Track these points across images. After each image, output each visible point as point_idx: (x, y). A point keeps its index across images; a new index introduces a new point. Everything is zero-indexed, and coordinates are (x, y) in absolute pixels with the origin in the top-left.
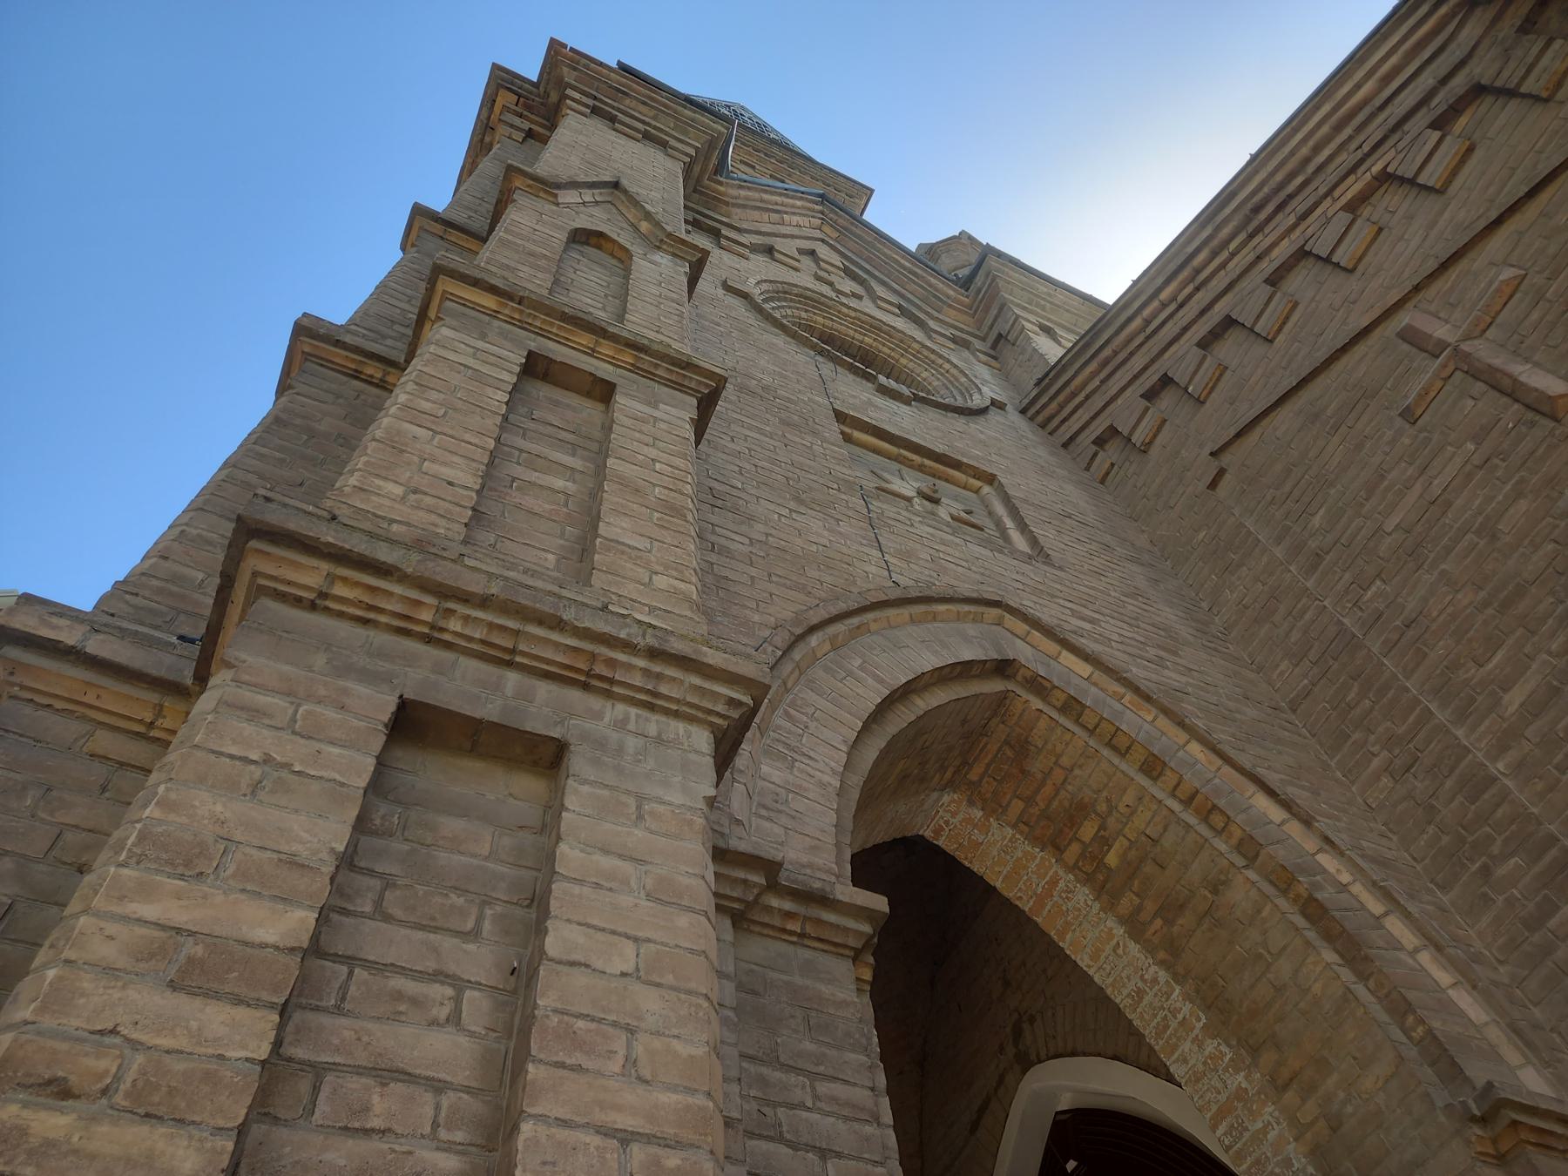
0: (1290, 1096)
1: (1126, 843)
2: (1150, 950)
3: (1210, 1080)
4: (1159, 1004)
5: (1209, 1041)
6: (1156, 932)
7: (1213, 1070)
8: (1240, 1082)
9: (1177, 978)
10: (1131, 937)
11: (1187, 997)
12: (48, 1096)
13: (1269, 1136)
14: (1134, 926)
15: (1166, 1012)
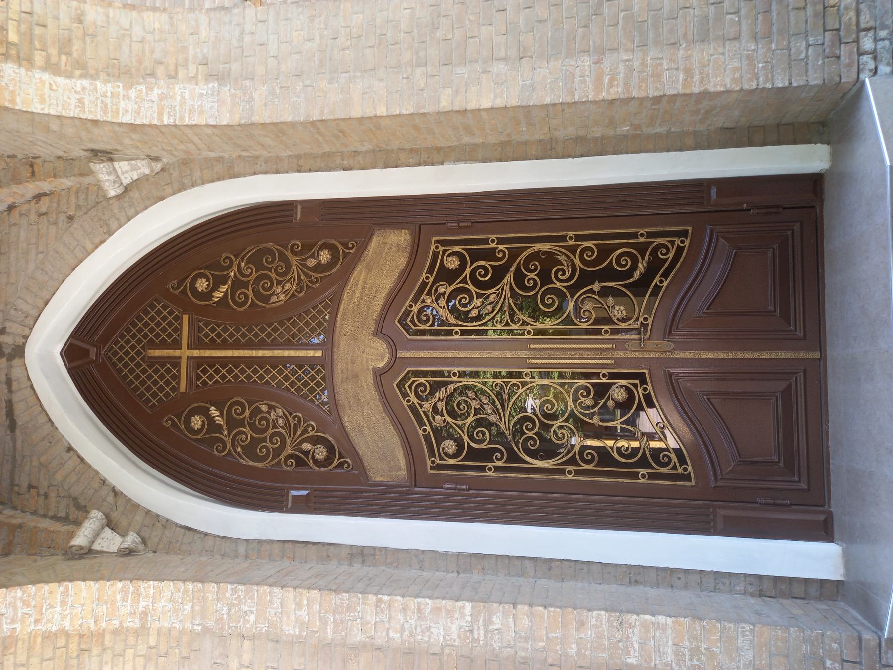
0: (181, 73)
1: (15, 23)
2: (70, 76)
3: (144, 107)
4: (95, 97)
5: (131, 91)
6: (66, 64)
7: (142, 102)
8: (157, 93)
9: (94, 77)
10: (54, 75)
11: (106, 82)
12: (693, 594)
13: (186, 98)
14: (51, 67)
15: (101, 98)
